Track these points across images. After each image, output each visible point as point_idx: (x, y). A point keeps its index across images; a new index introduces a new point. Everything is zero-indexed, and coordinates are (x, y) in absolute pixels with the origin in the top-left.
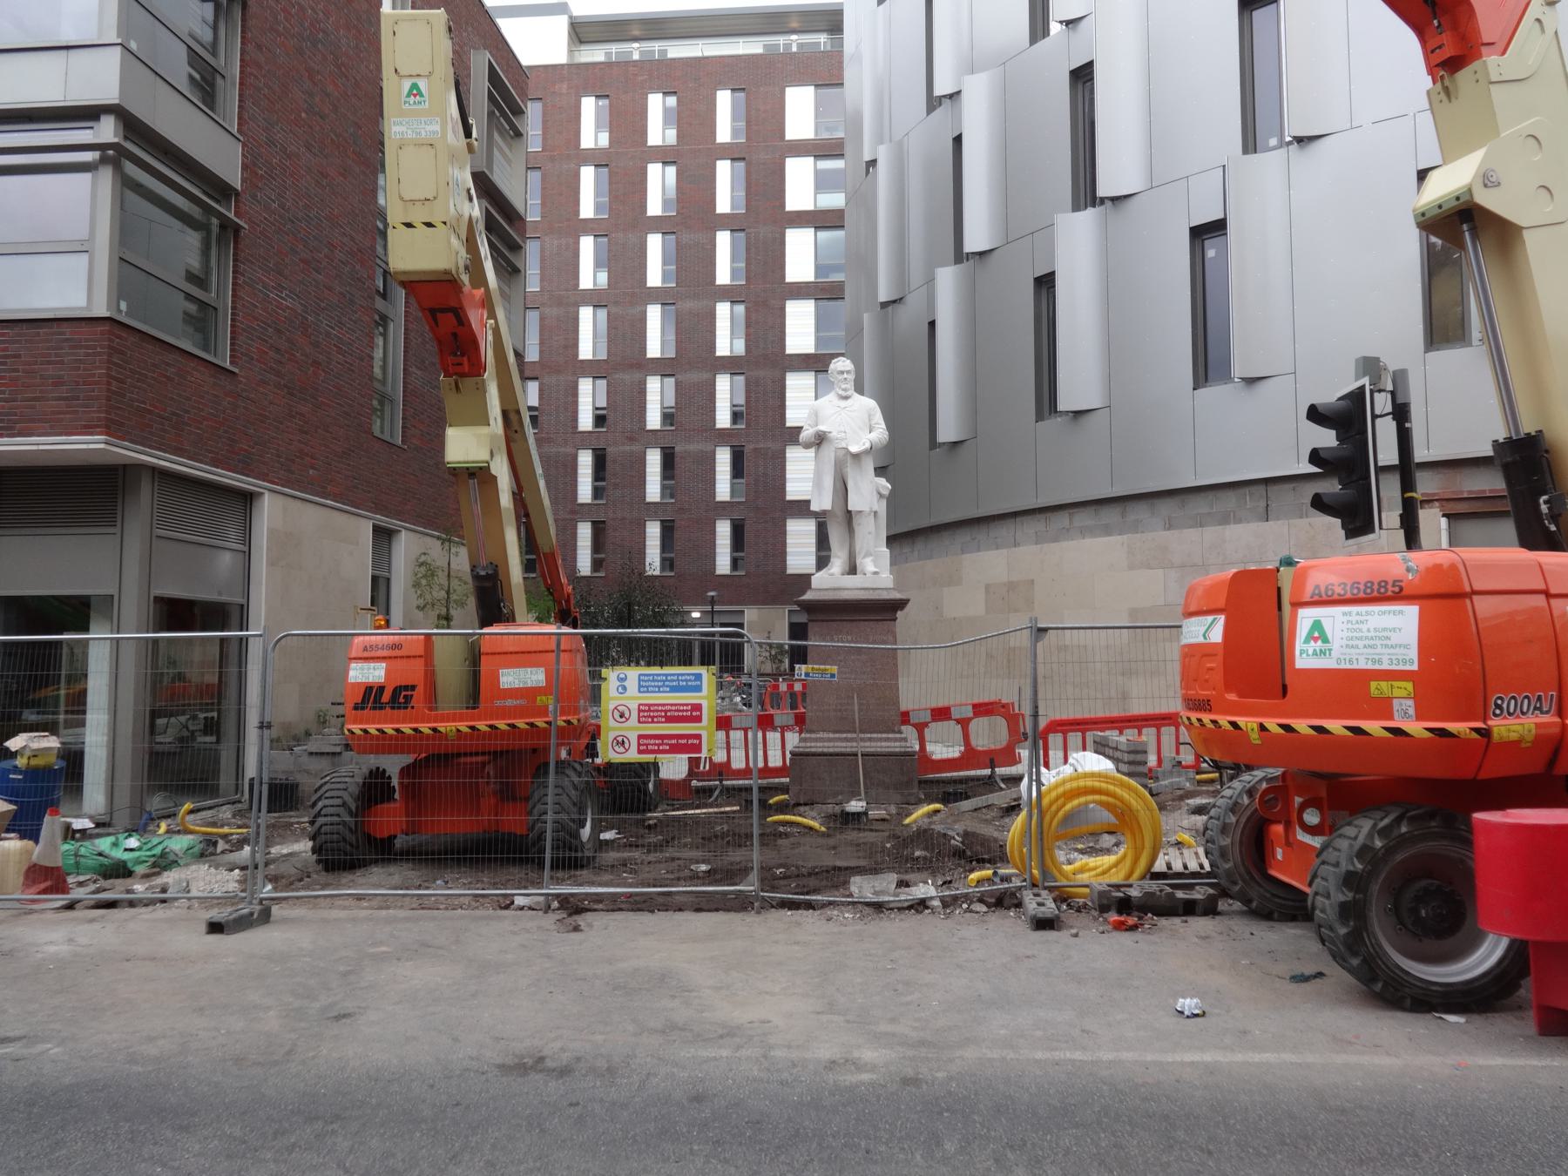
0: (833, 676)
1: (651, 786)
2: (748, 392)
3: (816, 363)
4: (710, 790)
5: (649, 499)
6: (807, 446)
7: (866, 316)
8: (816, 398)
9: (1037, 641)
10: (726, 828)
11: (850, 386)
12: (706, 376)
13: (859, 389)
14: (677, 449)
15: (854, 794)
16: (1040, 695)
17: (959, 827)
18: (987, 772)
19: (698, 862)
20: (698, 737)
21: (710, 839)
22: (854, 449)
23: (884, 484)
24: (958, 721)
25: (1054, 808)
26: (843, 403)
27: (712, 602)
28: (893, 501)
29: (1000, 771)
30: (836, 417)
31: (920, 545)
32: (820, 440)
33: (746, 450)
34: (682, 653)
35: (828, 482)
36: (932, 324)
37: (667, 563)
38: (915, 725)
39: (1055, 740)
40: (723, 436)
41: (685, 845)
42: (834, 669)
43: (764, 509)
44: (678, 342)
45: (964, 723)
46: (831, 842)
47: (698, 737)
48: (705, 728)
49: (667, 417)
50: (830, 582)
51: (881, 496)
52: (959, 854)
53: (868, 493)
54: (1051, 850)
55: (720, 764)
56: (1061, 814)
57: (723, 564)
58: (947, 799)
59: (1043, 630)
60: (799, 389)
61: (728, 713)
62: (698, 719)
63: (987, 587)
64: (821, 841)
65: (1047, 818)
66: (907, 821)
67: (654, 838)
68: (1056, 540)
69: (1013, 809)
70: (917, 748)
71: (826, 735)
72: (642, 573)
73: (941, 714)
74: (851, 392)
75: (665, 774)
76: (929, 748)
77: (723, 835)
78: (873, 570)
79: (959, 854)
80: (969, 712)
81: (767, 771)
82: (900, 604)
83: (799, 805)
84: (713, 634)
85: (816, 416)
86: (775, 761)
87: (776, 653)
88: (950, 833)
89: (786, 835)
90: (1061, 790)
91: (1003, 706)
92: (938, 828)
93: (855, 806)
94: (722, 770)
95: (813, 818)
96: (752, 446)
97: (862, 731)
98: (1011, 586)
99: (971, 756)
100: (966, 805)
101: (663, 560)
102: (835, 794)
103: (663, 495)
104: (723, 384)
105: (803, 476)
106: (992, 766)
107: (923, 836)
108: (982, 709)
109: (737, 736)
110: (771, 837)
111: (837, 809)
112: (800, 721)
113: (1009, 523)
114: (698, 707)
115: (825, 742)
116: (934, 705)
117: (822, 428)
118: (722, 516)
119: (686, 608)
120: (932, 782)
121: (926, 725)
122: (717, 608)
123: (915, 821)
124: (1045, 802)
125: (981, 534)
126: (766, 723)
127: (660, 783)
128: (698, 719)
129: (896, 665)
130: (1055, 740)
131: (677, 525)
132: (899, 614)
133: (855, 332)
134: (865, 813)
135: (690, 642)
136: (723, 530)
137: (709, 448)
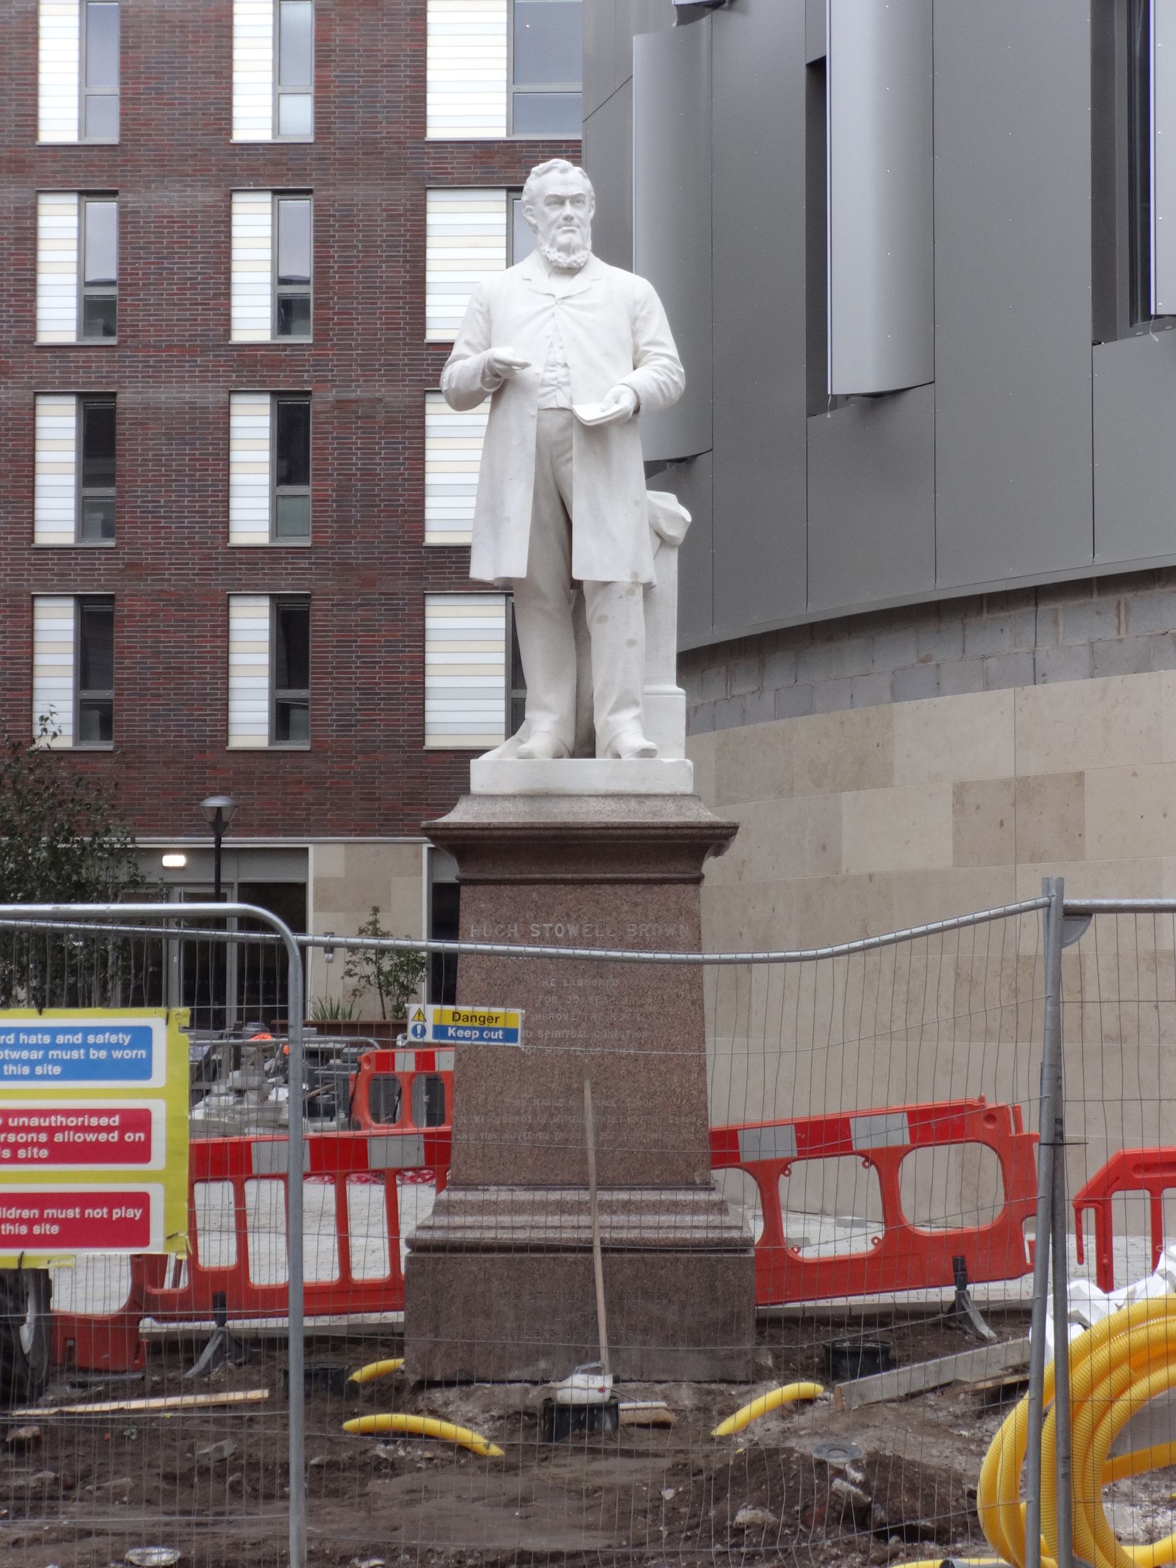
0: (510, 1035)
1: (26, 1334)
2: (322, 244)
3: (496, 166)
4: (192, 1346)
5: (43, 538)
6: (464, 401)
7: (638, 43)
8: (510, 261)
9: (1062, 942)
10: (228, 1447)
11: (582, 237)
12: (205, 197)
13: (613, 245)
14: (126, 398)
15: (582, 1358)
16: (1070, 1089)
17: (862, 1444)
18: (948, 1293)
19: (152, 1542)
20: (141, 1200)
21: (186, 1479)
22: (590, 412)
23: (672, 511)
24: (871, 1158)
25: (1101, 1392)
26: (562, 286)
27: (219, 824)
28: (698, 557)
29: (978, 1291)
30: (551, 321)
31: (780, 673)
32: (499, 383)
33: (316, 405)
34: (133, 972)
35: (519, 503)
36: (818, 69)
37: (94, 715)
38: (754, 1169)
39: (1129, 1206)
40: (250, 367)
41: (118, 1496)
42: (515, 1016)
43: (367, 571)
44: (128, 100)
45: (886, 1162)
46: (516, 1485)
47: (141, 1200)
48: (159, 1177)
49: (96, 311)
50: (512, 775)
51: (663, 541)
52: (857, 1516)
53: (628, 533)
54: (1093, 1504)
55: (219, 1275)
56: (1120, 1406)
57: (250, 720)
58: (832, 1367)
59: (1080, 914)
60: (461, 233)
61: (252, 1133)
62: (141, 1153)
63: (960, 791)
64: (488, 1482)
65: (1083, 1421)
66: (724, 1428)
67: (26, 1478)
68: (1143, 666)
69: (1001, 1397)
70: (756, 1229)
71: (504, 1195)
72: (21, 743)
73: (824, 1137)
74: (585, 254)
75: (64, 1301)
76: (792, 1228)
77: (222, 1468)
78: (646, 750)
79: (857, 1516)
80: (784, 1145)
81: (346, 1293)
82: (714, 839)
83: (434, 1384)
84: (219, 921)
85: (487, 318)
86: (372, 1264)
87: (396, 973)
88: (837, 1460)
89: (394, 1467)
90: (1120, 1343)
91: (991, 1116)
92: (806, 1446)
93: (583, 1387)
94: (226, 1290)
95: (469, 1422)
96: (331, 395)
97: (602, 1186)
98: (1024, 790)
99: (901, 1253)
100: (883, 1384)
101: (83, 707)
102: (530, 1358)
103: (82, 528)
104: (253, 220)
105: (464, 480)
106: (961, 1279)
107: (762, 1467)
108: (936, 1125)
109: (264, 1196)
110: (341, 1475)
111: (535, 1396)
112: (437, 1159)
113: (1021, 618)
114: (139, 1120)
115: (507, 1214)
116: (803, 1113)
117: (503, 352)
118: (250, 590)
119: (145, 842)
120: (792, 1321)
121: (783, 1166)
122: (229, 842)
123: (746, 1429)
124: (1079, 1375)
125: (942, 646)
126: (339, 1160)
127: (56, 1328)
128: (141, 1153)
129: (698, 1003)
130: (1129, 1206)
131: (121, 609)
132: (711, 866)
133: (609, 86)
134: (611, 1408)
135: (156, 944)
136: (251, 625)
137: (211, 397)
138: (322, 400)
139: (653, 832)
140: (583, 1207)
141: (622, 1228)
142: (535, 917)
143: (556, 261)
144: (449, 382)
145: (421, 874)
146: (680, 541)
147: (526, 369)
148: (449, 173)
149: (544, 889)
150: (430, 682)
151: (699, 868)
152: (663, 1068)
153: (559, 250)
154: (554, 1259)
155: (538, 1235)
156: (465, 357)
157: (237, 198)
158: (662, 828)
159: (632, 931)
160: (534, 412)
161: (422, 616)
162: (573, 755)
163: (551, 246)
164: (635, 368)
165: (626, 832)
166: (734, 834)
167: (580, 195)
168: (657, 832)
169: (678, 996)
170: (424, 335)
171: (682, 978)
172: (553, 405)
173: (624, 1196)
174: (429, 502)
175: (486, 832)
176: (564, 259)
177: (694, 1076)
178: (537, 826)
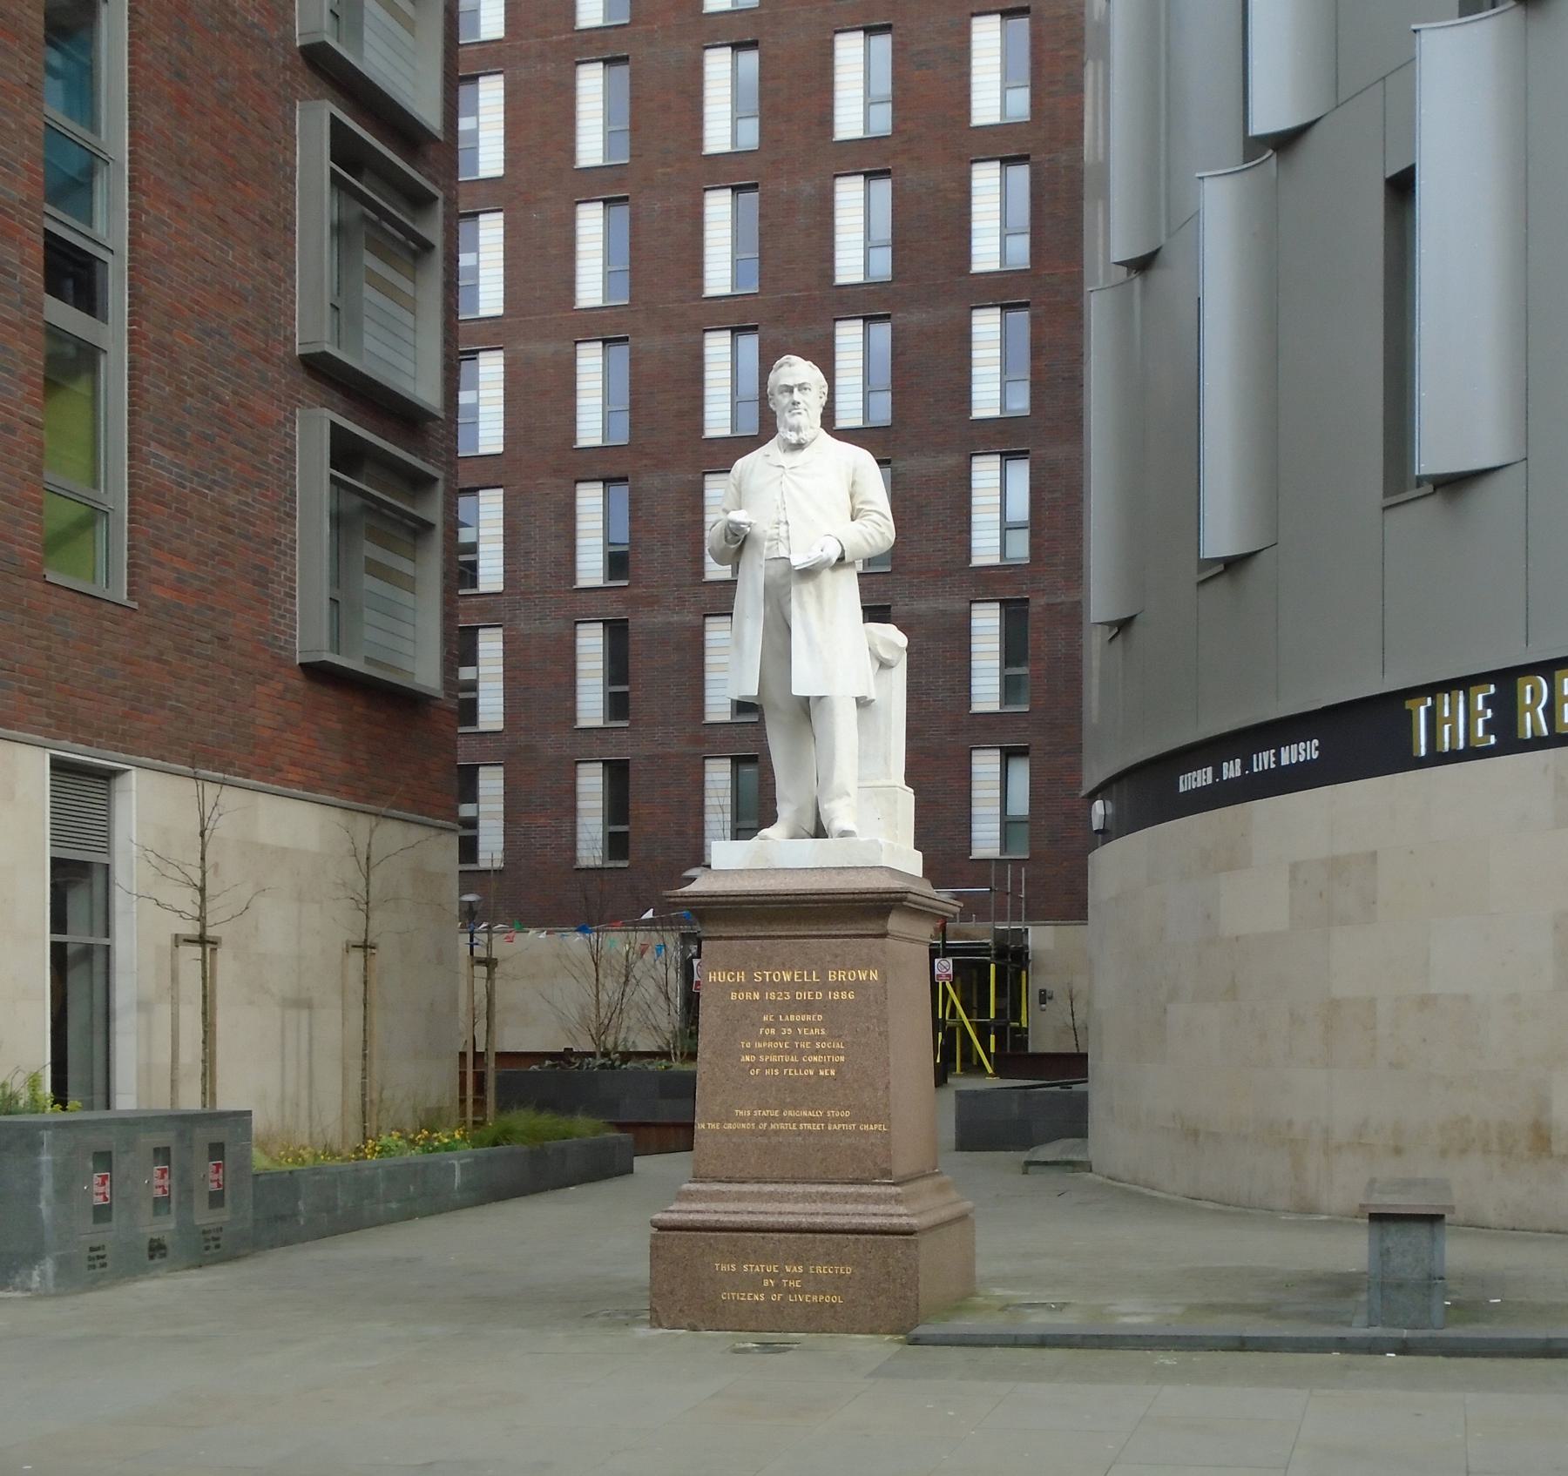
12: (951, 460)
37: (616, 844)
49: (617, 563)
63: (1295, 868)
96: (1043, 601)
138: (1037, 603)
155: (856, 1221)
157: (975, 459)
159: (831, 977)
160: (763, 562)
177: (880, 1093)
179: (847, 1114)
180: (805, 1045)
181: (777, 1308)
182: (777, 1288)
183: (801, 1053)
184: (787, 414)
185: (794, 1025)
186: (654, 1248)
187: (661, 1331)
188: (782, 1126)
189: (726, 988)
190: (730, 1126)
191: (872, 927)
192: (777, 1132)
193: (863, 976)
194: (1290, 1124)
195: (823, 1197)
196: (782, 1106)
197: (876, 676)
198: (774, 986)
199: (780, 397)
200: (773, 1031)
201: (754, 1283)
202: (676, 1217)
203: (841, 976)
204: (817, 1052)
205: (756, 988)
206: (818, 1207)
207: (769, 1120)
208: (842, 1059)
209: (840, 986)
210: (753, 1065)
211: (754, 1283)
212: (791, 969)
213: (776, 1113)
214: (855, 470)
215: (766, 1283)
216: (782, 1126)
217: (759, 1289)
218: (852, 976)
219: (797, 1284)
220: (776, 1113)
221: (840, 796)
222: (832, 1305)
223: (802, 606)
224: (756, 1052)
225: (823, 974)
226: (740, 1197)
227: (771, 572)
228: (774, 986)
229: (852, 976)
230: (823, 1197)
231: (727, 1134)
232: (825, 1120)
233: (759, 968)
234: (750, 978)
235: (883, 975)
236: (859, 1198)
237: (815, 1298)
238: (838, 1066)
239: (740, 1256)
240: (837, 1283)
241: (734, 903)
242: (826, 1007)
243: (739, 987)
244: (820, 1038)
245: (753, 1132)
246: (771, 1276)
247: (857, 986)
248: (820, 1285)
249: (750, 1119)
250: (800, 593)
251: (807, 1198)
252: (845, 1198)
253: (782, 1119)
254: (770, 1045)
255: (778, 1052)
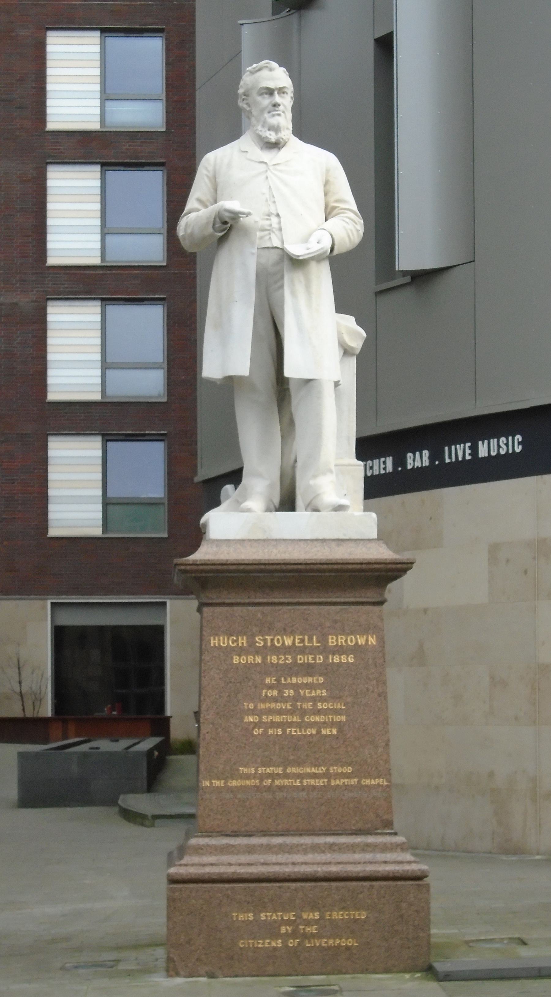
22: (297, 250)
26: (268, 156)
51: (346, 352)
63: (494, 550)
74: (287, 133)
117: (232, 204)
139: (350, 567)
140: (300, 848)
141: (330, 863)
142: (260, 632)
143: (267, 137)
144: (185, 230)
145: (47, 620)
146: (358, 352)
147: (250, 217)
148: (61, 152)
149: (267, 609)
150: (51, 492)
151: (382, 594)
152: (357, 744)
153: (269, 130)
154: (280, 887)
155: (370, 869)
156: (198, 210)
158: (358, 564)
160: (255, 251)
161: (45, 448)
162: (277, 510)
163: (263, 126)
164: (326, 220)
165: (330, 567)
166: (410, 568)
167: (284, 87)
168: (354, 566)
169: (368, 690)
170: (45, 261)
171: (371, 676)
172: (269, 245)
173: (330, 839)
174: (50, 372)
175: (225, 567)
176: (272, 137)
178: (263, 562)
179: (349, 770)
180: (308, 706)
181: (294, 952)
182: (294, 934)
183: (303, 713)
184: (266, 115)
185: (296, 687)
186: (171, 900)
187: (179, 980)
188: (286, 782)
189: (229, 652)
190: (234, 783)
191: (370, 595)
192: (281, 788)
193: (361, 641)
194: (491, 775)
195: (332, 847)
196: (286, 763)
197: (341, 361)
198: (276, 650)
199: (259, 99)
200: (275, 693)
201: (272, 930)
202: (193, 871)
203: (341, 640)
204: (319, 712)
205: (257, 651)
206: (328, 857)
207: (273, 776)
208: (343, 718)
209: (340, 650)
210: (256, 725)
211: (272, 930)
212: (292, 633)
213: (280, 770)
214: (328, 171)
215: (283, 930)
216: (286, 782)
217: (276, 935)
218: (351, 640)
219: (313, 929)
220: (280, 770)
221: (324, 474)
222: (348, 948)
223: (293, 294)
224: (261, 713)
225: (323, 639)
226: (251, 850)
227: (263, 261)
228: (276, 650)
229: (351, 640)
230: (332, 847)
231: (232, 790)
232: (326, 775)
233: (261, 633)
234: (252, 643)
235: (381, 640)
236: (366, 848)
237: (331, 942)
238: (340, 726)
239: (259, 905)
240: (352, 927)
241: (244, 571)
242: (327, 670)
243: (240, 651)
244: (322, 699)
245: (257, 789)
246: (289, 922)
247: (356, 650)
248: (336, 929)
249: (254, 776)
250: (292, 282)
251: (315, 848)
252: (352, 848)
253: (286, 776)
254: (273, 705)
255: (280, 712)
